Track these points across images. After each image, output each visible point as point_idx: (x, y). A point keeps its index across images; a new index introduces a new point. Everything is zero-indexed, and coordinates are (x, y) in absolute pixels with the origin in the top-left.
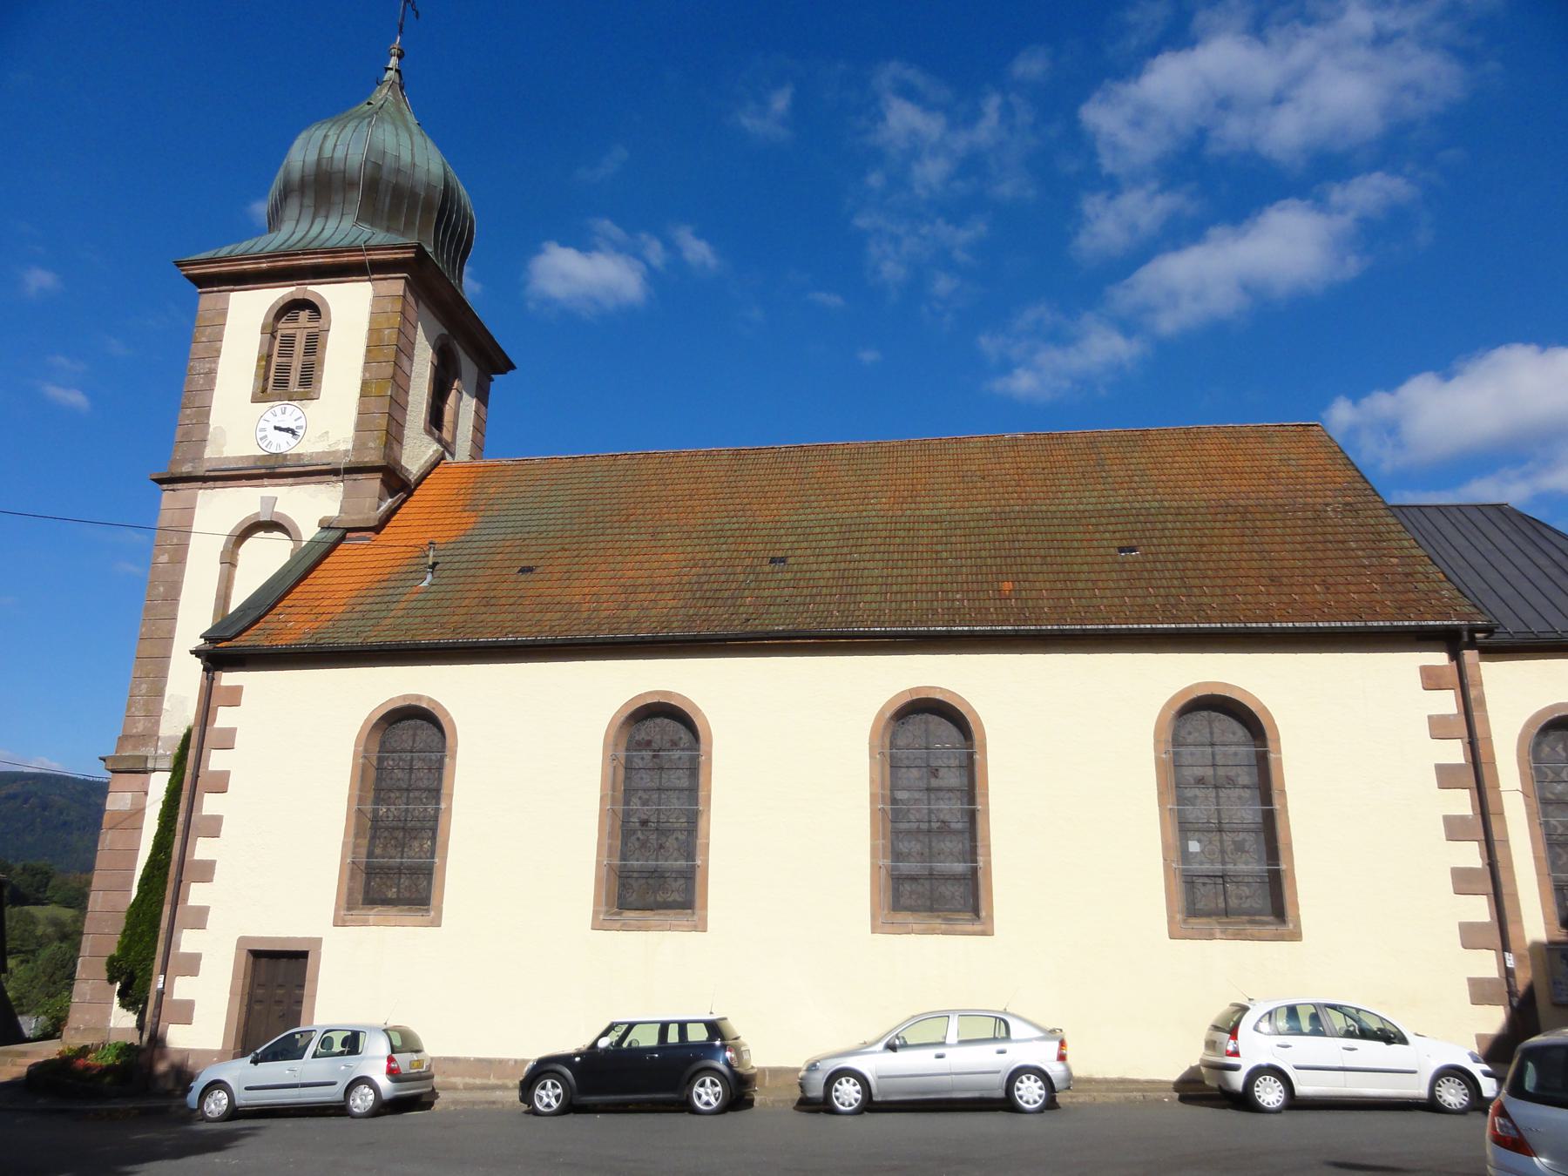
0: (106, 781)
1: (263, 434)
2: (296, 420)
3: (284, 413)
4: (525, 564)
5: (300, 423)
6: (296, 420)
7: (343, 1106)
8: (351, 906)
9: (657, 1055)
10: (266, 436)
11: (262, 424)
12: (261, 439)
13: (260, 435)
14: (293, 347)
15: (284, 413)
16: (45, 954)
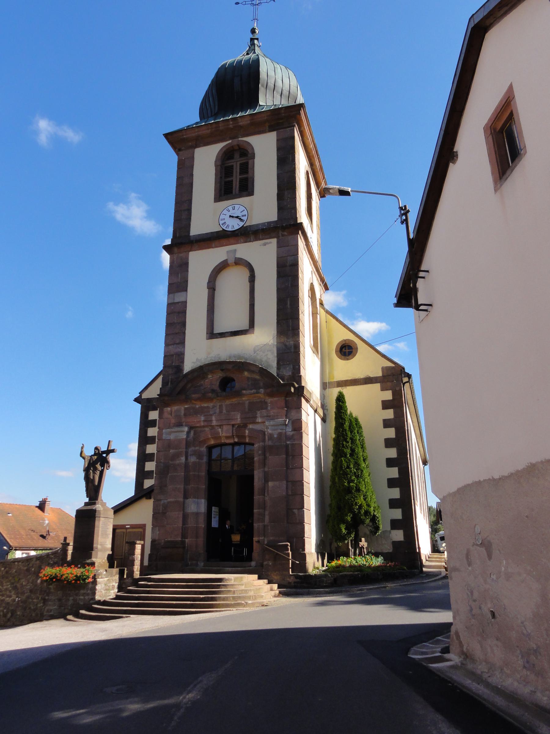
0: (443, 536)
1: (223, 221)
2: (241, 212)
3: (234, 209)
4: (496, 614)
5: (243, 213)
6: (241, 212)
7: (231, 192)
8: (220, 196)
9: (411, 672)
10: (225, 223)
11: (222, 217)
12: (222, 224)
13: (221, 222)
14: (232, 174)
15: (234, 209)
16: (26, 595)
